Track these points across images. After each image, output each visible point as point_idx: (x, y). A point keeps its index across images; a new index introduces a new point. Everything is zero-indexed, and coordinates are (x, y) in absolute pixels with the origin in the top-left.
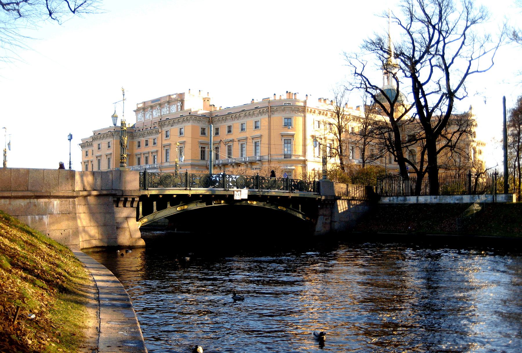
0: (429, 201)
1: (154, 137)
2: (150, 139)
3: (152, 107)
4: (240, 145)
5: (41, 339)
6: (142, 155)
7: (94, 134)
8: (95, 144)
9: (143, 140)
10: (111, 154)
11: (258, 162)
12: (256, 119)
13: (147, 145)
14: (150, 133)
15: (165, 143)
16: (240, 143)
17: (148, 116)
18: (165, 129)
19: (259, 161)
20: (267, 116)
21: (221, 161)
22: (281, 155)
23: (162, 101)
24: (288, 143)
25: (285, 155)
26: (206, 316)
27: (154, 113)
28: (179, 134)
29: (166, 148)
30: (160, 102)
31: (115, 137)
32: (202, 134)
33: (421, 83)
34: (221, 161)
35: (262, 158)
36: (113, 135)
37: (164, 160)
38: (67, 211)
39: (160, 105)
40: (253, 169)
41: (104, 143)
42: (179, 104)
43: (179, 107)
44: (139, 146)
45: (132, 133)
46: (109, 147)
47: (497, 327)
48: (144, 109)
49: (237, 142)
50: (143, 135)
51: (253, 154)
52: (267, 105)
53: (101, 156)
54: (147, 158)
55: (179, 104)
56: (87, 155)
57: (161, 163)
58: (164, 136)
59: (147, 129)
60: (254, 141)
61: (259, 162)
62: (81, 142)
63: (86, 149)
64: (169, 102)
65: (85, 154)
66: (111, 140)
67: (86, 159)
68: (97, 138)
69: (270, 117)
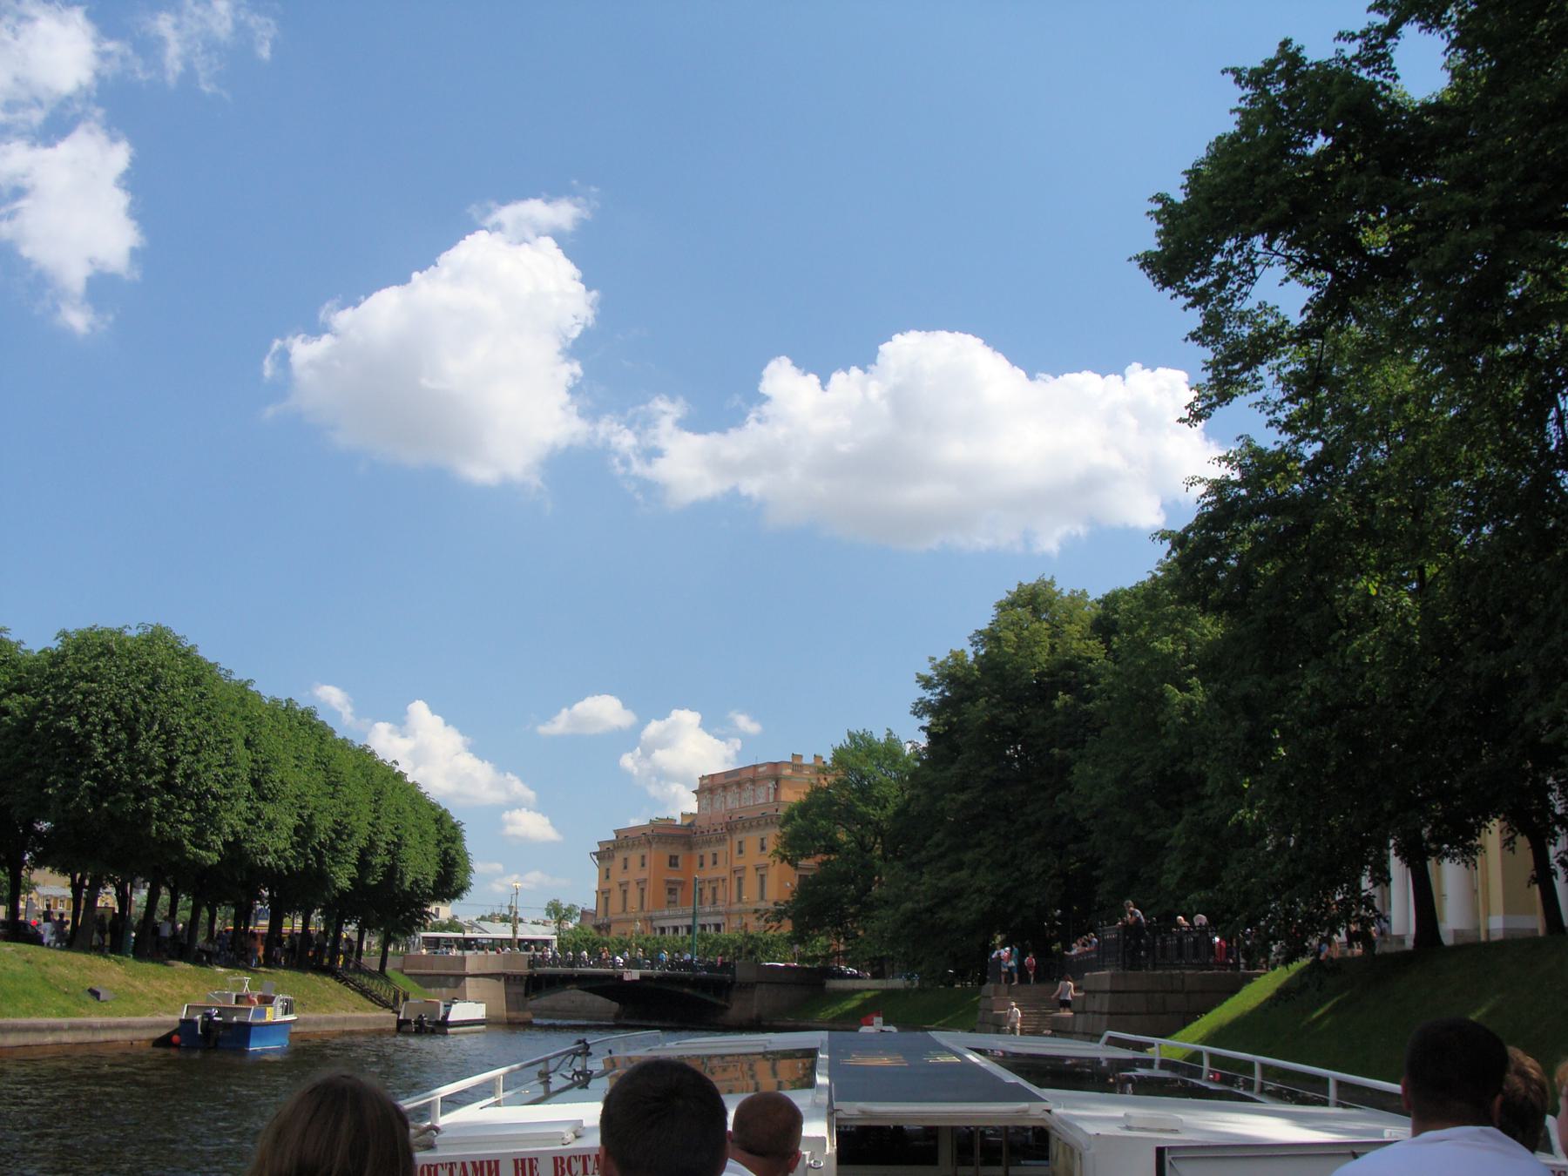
0: (982, 1065)
1: (714, 849)
2: (721, 850)
3: (725, 787)
5: (1011, 707)
6: (707, 884)
8: (619, 857)
9: (708, 852)
10: (645, 881)
14: (721, 840)
15: (737, 864)
17: (717, 805)
18: (738, 837)
23: (744, 775)
26: (1271, 116)
27: (729, 800)
28: (759, 849)
29: (739, 875)
30: (737, 779)
31: (654, 846)
32: (671, 865)
33: (119, 157)
36: (649, 842)
37: (735, 899)
39: (739, 784)
41: (634, 856)
42: (771, 785)
43: (772, 791)
44: (702, 865)
45: (689, 836)
46: (643, 865)
48: (711, 790)
50: (708, 843)
53: (627, 883)
54: (714, 889)
55: (771, 785)
56: (608, 877)
57: (730, 904)
58: (697, 862)
59: (715, 830)
62: (597, 849)
63: (607, 864)
64: (753, 781)
65: (604, 876)
66: (644, 851)
67: (606, 887)
68: (628, 846)
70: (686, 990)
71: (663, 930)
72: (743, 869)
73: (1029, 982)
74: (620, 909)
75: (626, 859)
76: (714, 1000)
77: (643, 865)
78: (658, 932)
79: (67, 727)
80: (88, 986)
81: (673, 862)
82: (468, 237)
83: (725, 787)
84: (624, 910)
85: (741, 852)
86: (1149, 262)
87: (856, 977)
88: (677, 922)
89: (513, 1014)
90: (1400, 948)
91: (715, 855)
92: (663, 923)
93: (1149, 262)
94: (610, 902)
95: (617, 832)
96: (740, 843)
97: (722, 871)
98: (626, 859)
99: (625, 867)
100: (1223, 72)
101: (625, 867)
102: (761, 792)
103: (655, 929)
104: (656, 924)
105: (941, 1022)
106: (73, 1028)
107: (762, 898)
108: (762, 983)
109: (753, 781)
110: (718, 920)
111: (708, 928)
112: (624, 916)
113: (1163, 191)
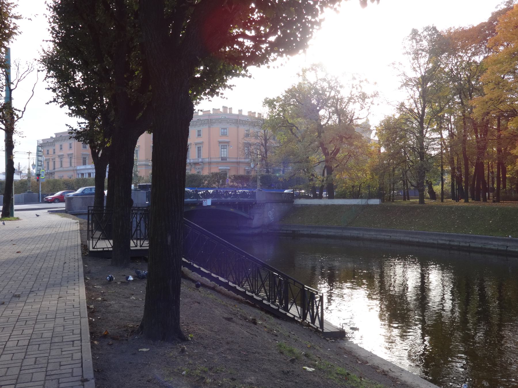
4: (197, 148)
7: (56, 136)
8: (57, 146)
10: (72, 154)
11: (200, 163)
12: (199, 129)
16: (47, 161)
19: (201, 162)
20: (207, 127)
21: (192, 161)
22: (219, 158)
24: (224, 149)
25: (222, 158)
34: (192, 161)
35: (203, 160)
38: (271, 161)
40: (196, 169)
46: (71, 147)
47: (434, 151)
49: (194, 146)
51: (197, 157)
52: (207, 118)
60: (47, 161)
61: (202, 163)
69: (209, 127)
70: (232, 210)
71: (83, 174)
73: (480, 200)
74: (59, 166)
75: (61, 145)
76: (244, 214)
77: (71, 147)
78: (80, 175)
82: (231, 81)
84: (61, 166)
86: (303, 69)
87: (308, 197)
89: (481, 199)
90: (93, 200)
92: (82, 172)
93: (303, 69)
95: (56, 134)
98: (61, 145)
99: (61, 149)
100: (44, 14)
101: (61, 149)
103: (79, 174)
104: (78, 172)
108: (268, 203)
111: (85, 175)
112: (61, 169)
113: (276, 61)
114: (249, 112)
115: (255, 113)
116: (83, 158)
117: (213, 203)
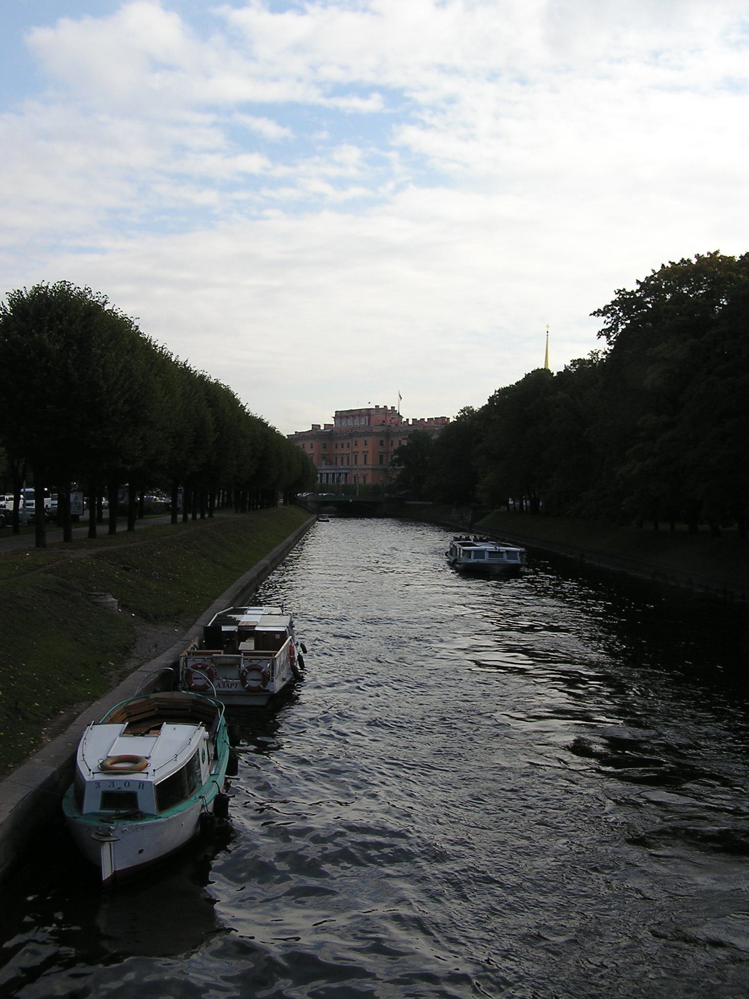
2: (345, 442)
3: (347, 417)
13: (342, 447)
18: (355, 439)
37: (354, 464)
42: (367, 417)
46: (312, 447)
54: (342, 457)
64: (359, 415)
72: (357, 452)
79: (633, 661)
80: (137, 852)
81: (381, 443)
83: (347, 417)
84: (365, 463)
85: (356, 445)
86: (683, 259)
88: (328, 472)
91: (342, 444)
93: (683, 259)
94: (358, 457)
96: (356, 442)
97: (346, 451)
102: (363, 420)
105: (247, 507)
106: (394, 910)
107: (365, 463)
109: (359, 415)
110: (346, 471)
114: (376, 406)
115: (319, 426)
116: (380, 456)
117: (353, 501)
